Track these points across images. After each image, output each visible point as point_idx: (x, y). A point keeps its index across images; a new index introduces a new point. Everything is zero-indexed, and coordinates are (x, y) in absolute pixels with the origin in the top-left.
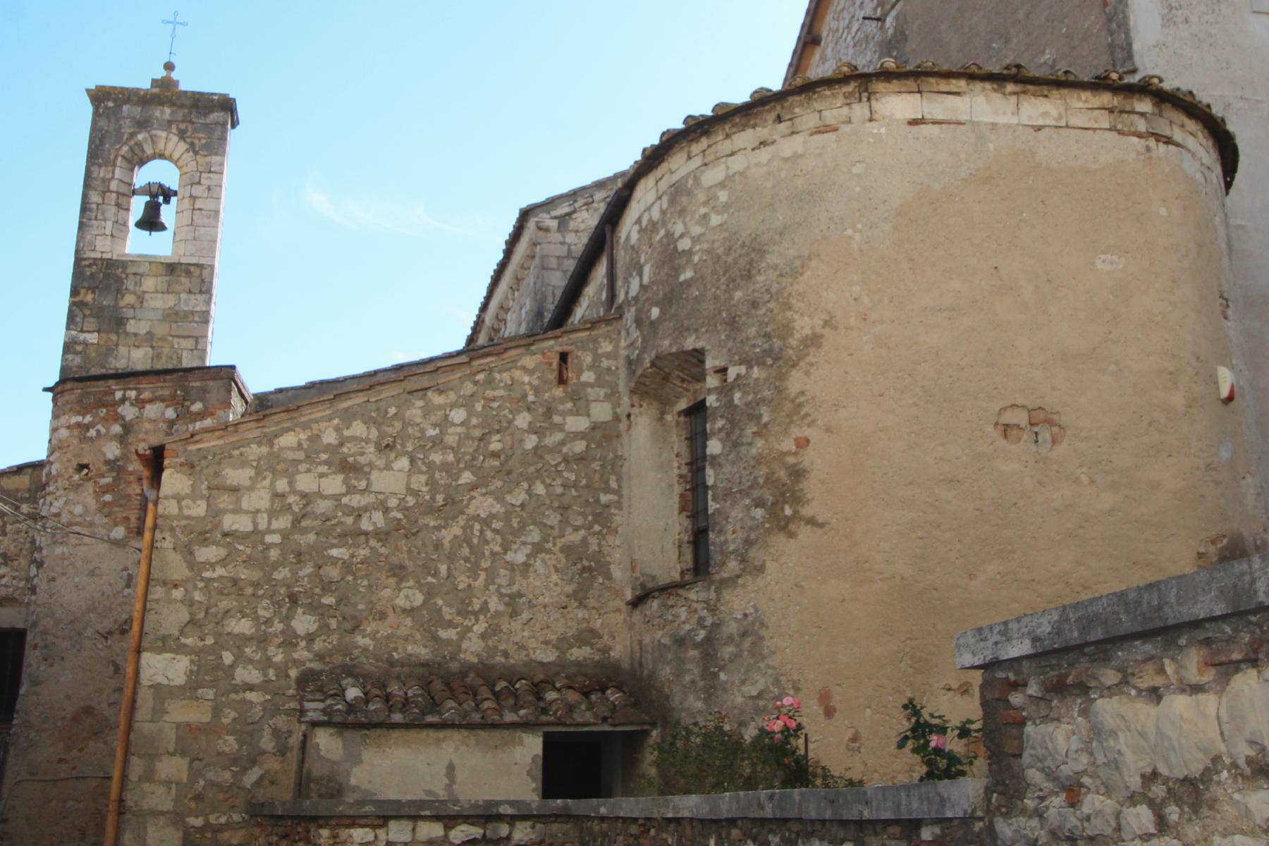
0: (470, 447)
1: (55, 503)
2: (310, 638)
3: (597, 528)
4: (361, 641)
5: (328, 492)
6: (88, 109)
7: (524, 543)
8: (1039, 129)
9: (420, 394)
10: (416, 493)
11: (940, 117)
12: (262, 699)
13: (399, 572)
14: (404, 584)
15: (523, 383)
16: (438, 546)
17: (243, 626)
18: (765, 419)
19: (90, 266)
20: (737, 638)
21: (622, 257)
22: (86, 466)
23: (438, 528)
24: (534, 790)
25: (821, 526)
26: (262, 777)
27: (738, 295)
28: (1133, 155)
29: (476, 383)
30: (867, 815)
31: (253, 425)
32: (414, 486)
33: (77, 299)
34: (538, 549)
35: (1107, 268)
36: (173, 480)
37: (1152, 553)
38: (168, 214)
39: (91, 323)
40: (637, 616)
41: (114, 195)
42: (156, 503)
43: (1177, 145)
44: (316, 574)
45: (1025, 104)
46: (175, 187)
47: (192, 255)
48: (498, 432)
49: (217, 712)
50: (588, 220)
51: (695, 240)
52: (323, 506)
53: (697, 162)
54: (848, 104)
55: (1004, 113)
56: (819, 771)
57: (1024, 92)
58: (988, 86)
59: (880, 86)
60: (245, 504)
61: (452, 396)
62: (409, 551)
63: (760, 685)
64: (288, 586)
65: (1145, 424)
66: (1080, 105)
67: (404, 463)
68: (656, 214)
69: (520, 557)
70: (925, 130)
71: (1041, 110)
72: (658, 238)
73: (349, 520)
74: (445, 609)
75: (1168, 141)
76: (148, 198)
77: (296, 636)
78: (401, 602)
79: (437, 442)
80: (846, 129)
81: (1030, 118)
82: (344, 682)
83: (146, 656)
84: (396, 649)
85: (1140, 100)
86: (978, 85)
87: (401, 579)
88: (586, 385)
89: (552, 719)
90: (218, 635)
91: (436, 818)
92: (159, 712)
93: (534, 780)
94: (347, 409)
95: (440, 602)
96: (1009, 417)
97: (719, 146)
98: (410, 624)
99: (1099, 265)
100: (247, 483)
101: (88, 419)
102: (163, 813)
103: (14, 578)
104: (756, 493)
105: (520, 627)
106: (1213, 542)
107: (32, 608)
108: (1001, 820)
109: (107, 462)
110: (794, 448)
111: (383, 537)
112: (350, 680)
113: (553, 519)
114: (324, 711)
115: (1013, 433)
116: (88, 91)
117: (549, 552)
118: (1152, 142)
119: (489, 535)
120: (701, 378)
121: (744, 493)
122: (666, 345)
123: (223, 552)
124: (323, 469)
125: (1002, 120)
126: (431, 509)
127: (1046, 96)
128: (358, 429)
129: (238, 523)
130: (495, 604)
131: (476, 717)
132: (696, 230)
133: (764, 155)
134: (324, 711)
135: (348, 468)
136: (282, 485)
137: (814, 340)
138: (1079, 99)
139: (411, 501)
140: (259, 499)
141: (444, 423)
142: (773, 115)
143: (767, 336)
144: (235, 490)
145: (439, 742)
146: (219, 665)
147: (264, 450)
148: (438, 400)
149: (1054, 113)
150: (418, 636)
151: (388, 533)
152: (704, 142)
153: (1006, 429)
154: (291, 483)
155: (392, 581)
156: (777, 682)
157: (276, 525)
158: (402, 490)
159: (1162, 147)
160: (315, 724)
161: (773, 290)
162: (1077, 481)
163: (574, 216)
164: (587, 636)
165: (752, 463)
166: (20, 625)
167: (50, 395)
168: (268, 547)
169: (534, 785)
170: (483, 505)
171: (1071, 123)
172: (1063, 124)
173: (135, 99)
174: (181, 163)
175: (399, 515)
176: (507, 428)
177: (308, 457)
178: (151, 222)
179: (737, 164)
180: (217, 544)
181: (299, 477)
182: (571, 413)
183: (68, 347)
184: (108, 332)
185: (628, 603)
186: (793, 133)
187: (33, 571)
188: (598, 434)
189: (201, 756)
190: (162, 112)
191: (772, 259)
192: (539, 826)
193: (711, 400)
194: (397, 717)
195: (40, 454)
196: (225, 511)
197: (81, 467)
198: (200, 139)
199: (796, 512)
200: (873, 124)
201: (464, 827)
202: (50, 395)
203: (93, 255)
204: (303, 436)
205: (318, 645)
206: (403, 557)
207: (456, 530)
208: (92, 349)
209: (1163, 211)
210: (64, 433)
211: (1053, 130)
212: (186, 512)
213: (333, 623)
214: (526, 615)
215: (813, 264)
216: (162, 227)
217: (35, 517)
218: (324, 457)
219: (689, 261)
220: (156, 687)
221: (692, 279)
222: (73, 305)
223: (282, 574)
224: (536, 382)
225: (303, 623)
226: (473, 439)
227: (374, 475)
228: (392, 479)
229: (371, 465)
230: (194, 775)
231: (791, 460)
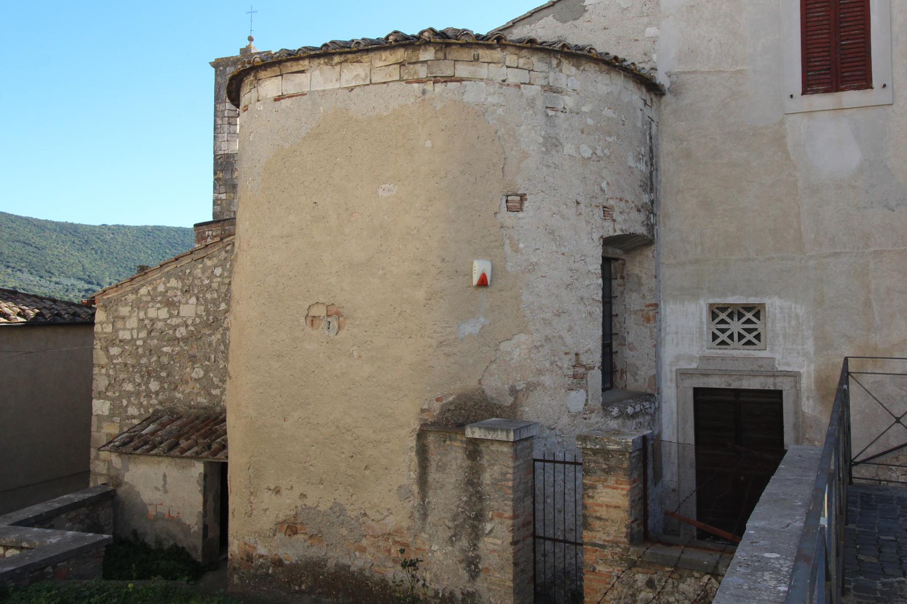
2: (157, 393)
4: (179, 395)
5: (161, 317)
8: (351, 89)
10: (200, 316)
11: (292, 92)
13: (193, 359)
16: (210, 345)
17: (129, 387)
23: (210, 335)
29: (227, 252)
31: (128, 284)
32: (199, 313)
35: (386, 194)
39: (222, 189)
44: (158, 361)
45: (345, 71)
49: (121, 427)
52: (159, 325)
55: (331, 81)
56: (657, 404)
57: (346, 61)
61: (215, 260)
64: (147, 367)
65: (397, 314)
66: (382, 64)
70: (285, 103)
71: (355, 73)
73: (171, 332)
77: (151, 392)
78: (194, 375)
79: (209, 287)
86: (316, 62)
87: (194, 363)
90: (120, 392)
92: (100, 428)
95: (212, 375)
96: (315, 312)
99: (380, 192)
100: (128, 314)
102: (103, 475)
106: (438, 400)
115: (316, 322)
123: (120, 350)
124: (158, 305)
125: (330, 86)
126: (208, 325)
128: (173, 283)
129: (125, 335)
135: (170, 304)
136: (142, 315)
138: (380, 59)
140: (133, 323)
141: (212, 276)
144: (123, 318)
145: (160, 462)
146: (121, 406)
147: (134, 296)
148: (209, 263)
149: (363, 74)
151: (187, 339)
153: (313, 320)
154: (146, 314)
155: (190, 364)
159: (439, 87)
162: (351, 355)
172: (368, 82)
175: (193, 329)
177: (152, 299)
180: (118, 346)
181: (149, 310)
183: (215, 203)
196: (120, 329)
204: (150, 288)
205: (160, 397)
206: (194, 351)
209: (429, 144)
212: (105, 330)
213: (166, 386)
218: (159, 298)
222: (215, 179)
223: (144, 361)
225: (154, 386)
226: (225, 284)
227: (182, 307)
228: (189, 309)
229: (179, 302)
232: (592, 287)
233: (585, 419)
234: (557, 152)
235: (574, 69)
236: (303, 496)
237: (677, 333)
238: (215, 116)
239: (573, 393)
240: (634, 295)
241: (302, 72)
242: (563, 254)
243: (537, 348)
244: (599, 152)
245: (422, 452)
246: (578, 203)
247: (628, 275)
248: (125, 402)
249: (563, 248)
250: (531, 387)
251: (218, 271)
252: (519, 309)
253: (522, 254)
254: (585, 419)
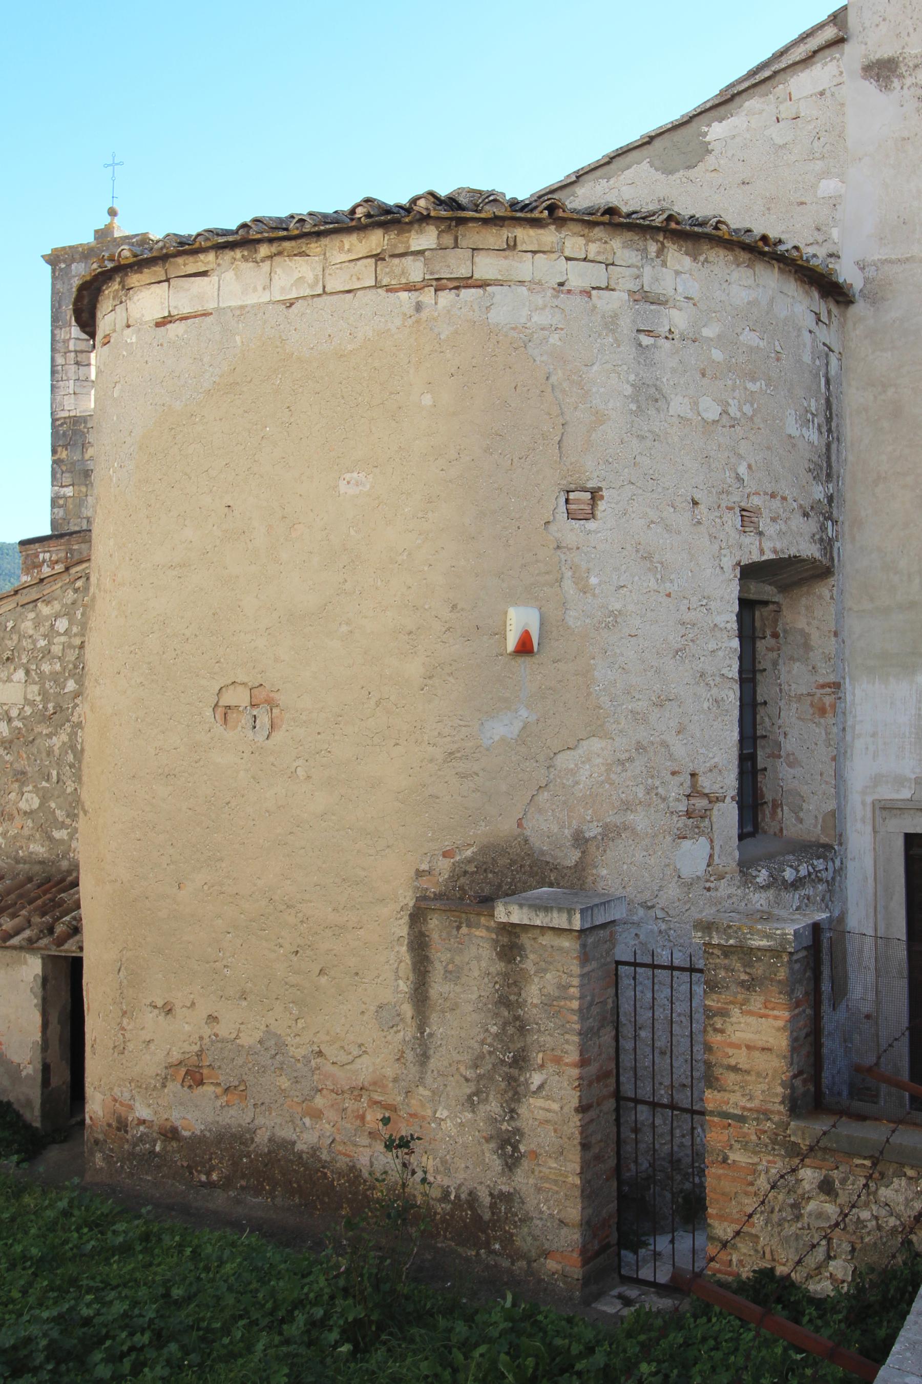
9: (31, 606)
10: (32, 703)
13: (21, 777)
14: (25, 789)
19: (62, 425)
23: (50, 736)
24: (36, 1006)
28: (398, 322)
32: (30, 697)
33: (55, 458)
37: (364, 869)
41: (73, 354)
45: (279, 271)
57: (280, 253)
61: (57, 606)
62: (28, 758)
65: (372, 702)
67: (20, 675)
71: (297, 275)
74: (58, 812)
78: (23, 805)
81: (283, 289)
84: (21, 848)
86: (228, 255)
87: (23, 784)
93: (36, 997)
95: (53, 805)
96: (228, 699)
98: (31, 825)
99: (343, 487)
108: (468, 1091)
111: (7, 745)
116: (42, 256)
125: (251, 299)
126: (47, 719)
138: (341, 249)
148: (45, 610)
150: (38, 836)
151: (11, 742)
153: (226, 713)
155: (16, 785)
159: (446, 298)
169: (35, 1001)
173: (77, 256)
175: (20, 725)
183: (54, 503)
184: (79, 485)
206: (22, 764)
208: (70, 500)
222: (54, 462)
232: (720, 653)
233: (709, 889)
234: (658, 410)
235: (687, 261)
237: (874, 735)
239: (686, 844)
240: (797, 667)
241: (204, 274)
242: (669, 595)
243: (621, 762)
244: (733, 411)
246: (695, 503)
247: (785, 631)
249: (668, 585)
250: (611, 833)
252: (589, 694)
253: (594, 595)
254: (709, 889)
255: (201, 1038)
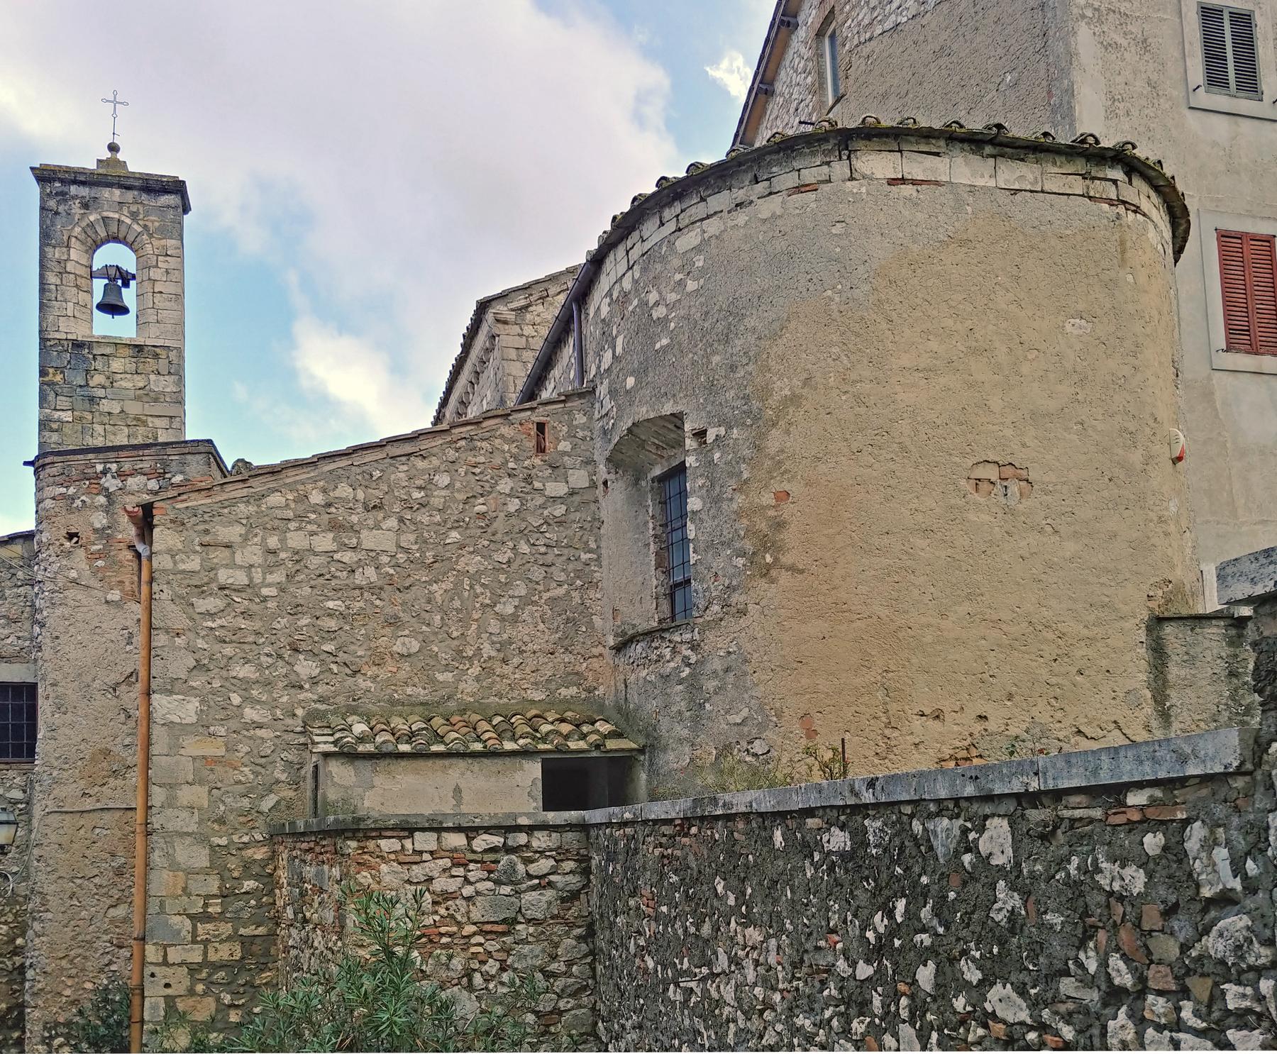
0: (455, 509)
1: (50, 566)
2: (314, 681)
3: (579, 583)
6: (35, 189)
7: (513, 597)
8: (1016, 192)
12: (272, 735)
15: (503, 451)
17: (245, 672)
18: (745, 476)
20: (721, 673)
21: (591, 330)
22: (76, 535)
25: (802, 572)
26: (278, 803)
27: (716, 359)
30: (1034, 785)
34: (526, 601)
36: (163, 537)
38: (129, 296)
40: (621, 661)
42: (150, 559)
43: (1144, 215)
45: (1003, 167)
46: (133, 270)
47: (157, 337)
48: (482, 495)
50: (547, 313)
51: (671, 307)
53: (671, 227)
54: (828, 163)
58: (966, 146)
59: (859, 144)
60: (239, 559)
61: (436, 461)
63: (745, 712)
66: (1056, 170)
67: (392, 523)
68: (627, 284)
69: (510, 610)
71: (1018, 174)
72: (630, 308)
75: (1137, 210)
76: (106, 281)
80: (826, 188)
81: (1007, 181)
82: (349, 720)
83: (155, 697)
85: (1112, 167)
88: (564, 453)
89: (549, 747)
91: (458, 829)
92: (175, 748)
94: (331, 472)
96: (982, 472)
97: (693, 210)
99: (1068, 328)
101: (72, 491)
103: (19, 638)
104: (737, 545)
105: (511, 670)
107: (40, 663)
109: (96, 531)
110: (773, 502)
112: (355, 718)
113: (538, 573)
114: (335, 743)
115: (984, 486)
116: (32, 169)
117: (534, 603)
118: (1121, 209)
119: (479, 589)
120: (680, 443)
121: (728, 544)
122: (643, 412)
125: (980, 182)
127: (1022, 160)
130: (488, 650)
131: (478, 747)
132: (672, 297)
133: (741, 217)
134: (335, 743)
136: (273, 542)
137: (794, 400)
138: (1054, 163)
139: (402, 557)
140: (251, 554)
142: (750, 176)
143: (746, 398)
148: (420, 464)
149: (1030, 177)
152: (677, 208)
154: (283, 540)
155: (388, 631)
156: (761, 709)
157: (270, 578)
158: (392, 548)
159: (1131, 215)
160: (326, 755)
161: (751, 354)
163: (531, 309)
164: (575, 677)
165: (733, 517)
166: (31, 680)
167: (31, 469)
168: (265, 599)
170: (472, 563)
171: (1046, 188)
174: (135, 246)
176: (490, 493)
178: (113, 308)
179: (713, 227)
182: (549, 478)
185: (612, 648)
186: (771, 194)
187: (37, 629)
188: (577, 498)
189: (219, 785)
190: (111, 193)
191: (750, 322)
192: (554, 835)
193: (690, 461)
194: (404, 748)
195: (29, 525)
197: (71, 536)
198: (153, 222)
199: (776, 560)
200: (854, 183)
201: (485, 837)
202: (31, 469)
203: (57, 336)
207: (447, 585)
210: (48, 503)
211: (1029, 194)
214: (516, 661)
215: (792, 325)
216: (124, 311)
217: (31, 582)
219: (666, 327)
220: (169, 725)
221: (668, 345)
222: (42, 384)
224: (515, 451)
230: (214, 803)
231: (772, 513)
236: (983, 718)
238: (43, 267)
241: (937, 154)
245: (1158, 652)
248: (236, 699)
251: (444, 480)
255: (971, 735)
